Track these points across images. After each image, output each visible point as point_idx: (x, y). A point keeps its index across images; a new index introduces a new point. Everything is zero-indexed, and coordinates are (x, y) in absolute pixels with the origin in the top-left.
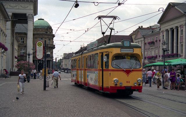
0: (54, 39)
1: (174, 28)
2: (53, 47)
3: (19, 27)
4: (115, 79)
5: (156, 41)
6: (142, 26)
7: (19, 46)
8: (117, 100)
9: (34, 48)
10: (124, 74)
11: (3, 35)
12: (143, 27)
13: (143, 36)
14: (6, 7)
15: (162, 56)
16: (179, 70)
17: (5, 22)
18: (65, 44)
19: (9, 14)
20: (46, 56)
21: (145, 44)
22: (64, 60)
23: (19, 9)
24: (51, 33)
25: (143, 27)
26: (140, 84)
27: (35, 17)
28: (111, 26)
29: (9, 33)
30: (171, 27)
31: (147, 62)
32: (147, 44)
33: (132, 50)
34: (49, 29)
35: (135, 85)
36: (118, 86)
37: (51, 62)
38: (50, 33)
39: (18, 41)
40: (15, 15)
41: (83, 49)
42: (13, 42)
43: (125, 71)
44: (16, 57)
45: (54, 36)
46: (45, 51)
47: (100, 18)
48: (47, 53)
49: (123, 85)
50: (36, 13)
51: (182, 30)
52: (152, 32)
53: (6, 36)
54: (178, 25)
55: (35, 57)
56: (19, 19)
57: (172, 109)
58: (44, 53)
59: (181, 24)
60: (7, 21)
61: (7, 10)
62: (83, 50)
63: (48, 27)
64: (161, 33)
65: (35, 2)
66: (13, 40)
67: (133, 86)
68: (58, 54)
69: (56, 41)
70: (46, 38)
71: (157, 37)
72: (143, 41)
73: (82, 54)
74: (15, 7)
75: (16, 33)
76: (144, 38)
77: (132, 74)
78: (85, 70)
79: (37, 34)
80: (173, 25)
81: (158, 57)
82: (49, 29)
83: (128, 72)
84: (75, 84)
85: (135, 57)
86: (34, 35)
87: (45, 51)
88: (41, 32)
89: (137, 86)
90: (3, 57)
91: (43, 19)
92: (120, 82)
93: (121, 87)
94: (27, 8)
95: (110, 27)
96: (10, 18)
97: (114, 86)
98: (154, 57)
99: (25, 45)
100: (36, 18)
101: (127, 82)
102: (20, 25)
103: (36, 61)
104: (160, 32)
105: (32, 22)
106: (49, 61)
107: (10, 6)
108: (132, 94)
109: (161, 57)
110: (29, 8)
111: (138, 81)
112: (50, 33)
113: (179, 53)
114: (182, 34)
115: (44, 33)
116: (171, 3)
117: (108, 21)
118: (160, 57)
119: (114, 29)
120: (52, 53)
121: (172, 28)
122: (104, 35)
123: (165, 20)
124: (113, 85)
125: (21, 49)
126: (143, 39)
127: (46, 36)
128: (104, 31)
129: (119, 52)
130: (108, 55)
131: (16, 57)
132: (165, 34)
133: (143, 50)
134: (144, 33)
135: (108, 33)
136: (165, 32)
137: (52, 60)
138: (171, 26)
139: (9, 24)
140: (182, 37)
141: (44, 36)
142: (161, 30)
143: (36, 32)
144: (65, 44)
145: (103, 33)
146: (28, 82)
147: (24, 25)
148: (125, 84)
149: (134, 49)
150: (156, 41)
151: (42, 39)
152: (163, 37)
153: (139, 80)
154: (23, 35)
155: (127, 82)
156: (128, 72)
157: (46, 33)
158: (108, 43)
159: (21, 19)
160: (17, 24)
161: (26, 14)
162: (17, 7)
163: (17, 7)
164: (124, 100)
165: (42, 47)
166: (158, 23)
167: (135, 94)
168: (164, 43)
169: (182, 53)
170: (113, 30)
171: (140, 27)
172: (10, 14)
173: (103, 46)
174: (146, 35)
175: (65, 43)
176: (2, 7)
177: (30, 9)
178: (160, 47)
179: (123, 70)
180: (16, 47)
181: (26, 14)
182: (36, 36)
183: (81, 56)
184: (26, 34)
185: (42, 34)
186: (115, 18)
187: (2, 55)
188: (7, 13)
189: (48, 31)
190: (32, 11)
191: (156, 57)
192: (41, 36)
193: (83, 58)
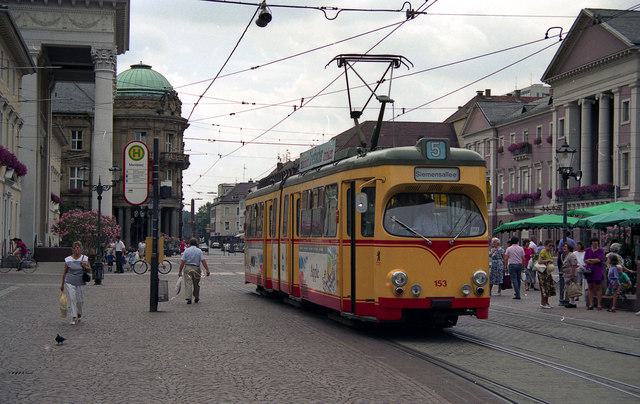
0: (187, 133)
1: (599, 96)
2: (184, 163)
3: (66, 94)
4: (395, 273)
5: (538, 142)
6: (488, 91)
7: (64, 160)
8: (403, 344)
9: (119, 167)
10: (426, 256)
11: (11, 121)
12: (492, 94)
13: (493, 124)
14: (19, 24)
15: (557, 194)
16: (614, 241)
17: (17, 77)
18: (223, 153)
19: (29, 48)
20: (157, 192)
21: (499, 151)
22: (220, 206)
23: (64, 30)
24: (176, 115)
25: (492, 94)
26: (481, 291)
27: (120, 58)
28: (382, 91)
29: (29, 112)
30: (588, 92)
31: (507, 213)
32: (506, 151)
33: (455, 171)
34: (170, 99)
35: (466, 295)
36: (407, 295)
37: (175, 215)
38: (173, 113)
39: (62, 143)
40: (51, 52)
41: (284, 169)
42: (46, 146)
43: (429, 246)
44: (54, 198)
45: (185, 124)
46: (155, 175)
47: (343, 61)
48: (163, 184)
49: (424, 295)
50: (122, 44)
51: (627, 104)
52: (524, 110)
53: (21, 125)
54: (612, 86)
55: (119, 196)
56: (65, 67)
57: (591, 376)
58: (153, 182)
59: (622, 81)
60: (25, 72)
61: (24, 35)
62: (284, 172)
63: (166, 92)
64: (554, 114)
65: (120, 7)
66: (45, 138)
67: (457, 296)
68: (198, 188)
69: (193, 141)
70: (157, 132)
71: (539, 129)
72: (492, 143)
73: (281, 188)
74: (50, 23)
75: (56, 114)
76: (497, 131)
77: (453, 255)
78: (293, 240)
79: (128, 118)
80: (594, 85)
81: (544, 196)
82: (170, 99)
83: (440, 248)
84: (260, 288)
85: (463, 196)
86: (116, 120)
87: (155, 175)
88: (143, 112)
89: (472, 296)
90: (9, 195)
91: (149, 67)
92: (412, 282)
93: (416, 300)
94: (92, 29)
95: (379, 93)
96: (35, 61)
97: (393, 297)
98: (531, 197)
99: (87, 155)
100: (123, 64)
101: (438, 283)
102: (70, 86)
103: (124, 212)
104: (551, 112)
105: (111, 76)
106: (170, 210)
107: (34, 20)
108: (455, 324)
109: (554, 197)
110: (99, 27)
111: (473, 279)
112: (173, 113)
113: (616, 183)
114: (626, 118)
115: (152, 112)
116: (589, 9)
117: (372, 71)
118: (550, 196)
119: (392, 101)
120: (179, 182)
121: (592, 98)
122: (356, 122)
123: (569, 68)
124: (390, 295)
125: (73, 169)
126: (491, 135)
127: (157, 125)
128: (357, 107)
129: (411, 180)
130: (370, 192)
131: (54, 198)
132: (567, 118)
133: (491, 174)
134: (496, 113)
135: (370, 115)
136: (568, 111)
137: (179, 206)
138: (590, 89)
139: (31, 81)
140: (625, 129)
141: (151, 124)
142: (556, 103)
143: (122, 112)
144: (223, 153)
145: (355, 115)
146: (98, 282)
147: (83, 85)
148: (429, 291)
149: (462, 168)
150: (538, 142)
151: (144, 134)
152: (559, 127)
153: (477, 277)
154: (79, 122)
155: (438, 283)
156: (440, 248)
157: (157, 116)
158: (373, 149)
159: (73, 64)
160: (58, 85)
161: (89, 48)
162: (60, 25)
163: (60, 25)
164: (428, 345)
165: (145, 161)
166: (545, 78)
167: (465, 324)
168: (563, 149)
169: (626, 184)
170: (388, 105)
171: (480, 93)
172: (35, 48)
173: (354, 159)
174: (501, 122)
175: (225, 148)
176: (9, 25)
177: (104, 32)
178: (550, 162)
179: (424, 243)
180: (55, 162)
181: (89, 48)
182: (124, 124)
183: (277, 195)
184: (89, 118)
185: (146, 119)
186: (395, 61)
187: (8, 189)
188: (23, 46)
189: (166, 107)
190: (111, 39)
191: (536, 197)
192: (141, 125)
193: (286, 199)
